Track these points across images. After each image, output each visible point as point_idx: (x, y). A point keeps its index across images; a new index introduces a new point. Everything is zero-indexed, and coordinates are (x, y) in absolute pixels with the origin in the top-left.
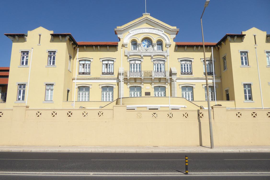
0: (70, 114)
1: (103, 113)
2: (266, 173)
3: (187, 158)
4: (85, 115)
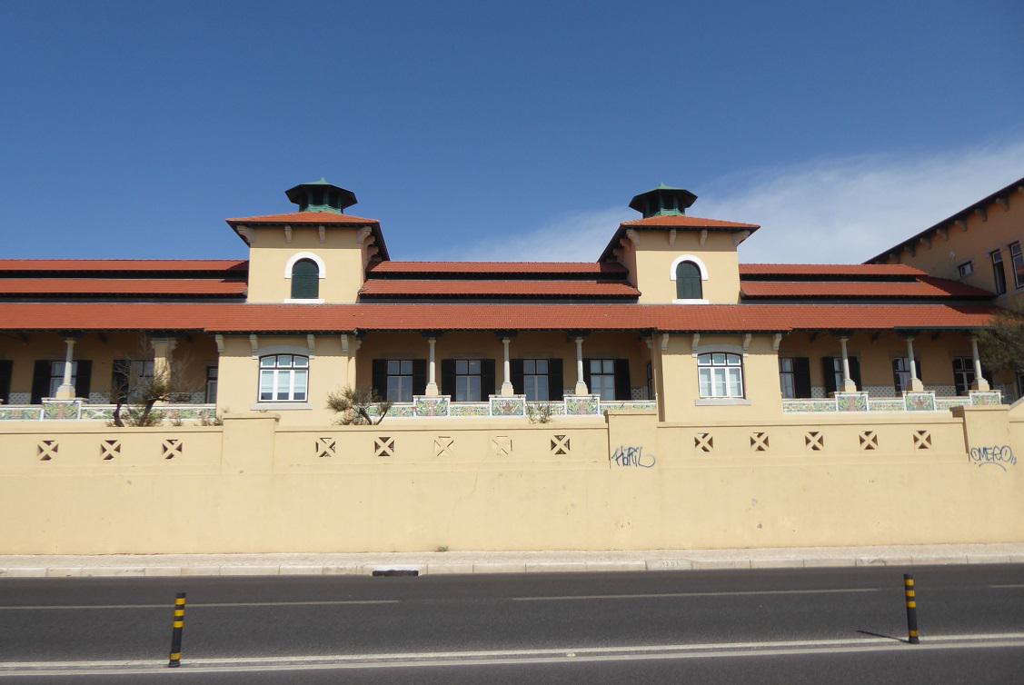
0: (48, 450)
1: (334, 444)
2: (1010, 639)
3: (911, 582)
4: (325, 453)
